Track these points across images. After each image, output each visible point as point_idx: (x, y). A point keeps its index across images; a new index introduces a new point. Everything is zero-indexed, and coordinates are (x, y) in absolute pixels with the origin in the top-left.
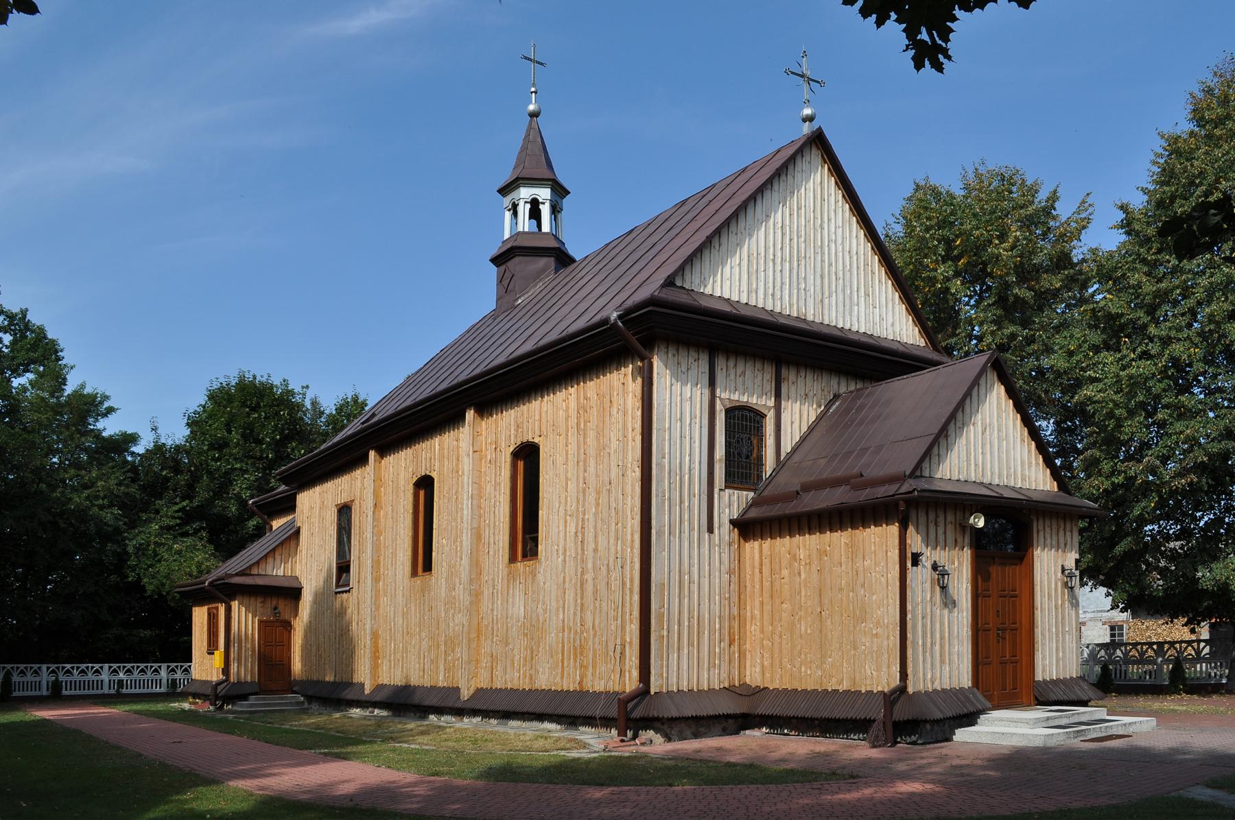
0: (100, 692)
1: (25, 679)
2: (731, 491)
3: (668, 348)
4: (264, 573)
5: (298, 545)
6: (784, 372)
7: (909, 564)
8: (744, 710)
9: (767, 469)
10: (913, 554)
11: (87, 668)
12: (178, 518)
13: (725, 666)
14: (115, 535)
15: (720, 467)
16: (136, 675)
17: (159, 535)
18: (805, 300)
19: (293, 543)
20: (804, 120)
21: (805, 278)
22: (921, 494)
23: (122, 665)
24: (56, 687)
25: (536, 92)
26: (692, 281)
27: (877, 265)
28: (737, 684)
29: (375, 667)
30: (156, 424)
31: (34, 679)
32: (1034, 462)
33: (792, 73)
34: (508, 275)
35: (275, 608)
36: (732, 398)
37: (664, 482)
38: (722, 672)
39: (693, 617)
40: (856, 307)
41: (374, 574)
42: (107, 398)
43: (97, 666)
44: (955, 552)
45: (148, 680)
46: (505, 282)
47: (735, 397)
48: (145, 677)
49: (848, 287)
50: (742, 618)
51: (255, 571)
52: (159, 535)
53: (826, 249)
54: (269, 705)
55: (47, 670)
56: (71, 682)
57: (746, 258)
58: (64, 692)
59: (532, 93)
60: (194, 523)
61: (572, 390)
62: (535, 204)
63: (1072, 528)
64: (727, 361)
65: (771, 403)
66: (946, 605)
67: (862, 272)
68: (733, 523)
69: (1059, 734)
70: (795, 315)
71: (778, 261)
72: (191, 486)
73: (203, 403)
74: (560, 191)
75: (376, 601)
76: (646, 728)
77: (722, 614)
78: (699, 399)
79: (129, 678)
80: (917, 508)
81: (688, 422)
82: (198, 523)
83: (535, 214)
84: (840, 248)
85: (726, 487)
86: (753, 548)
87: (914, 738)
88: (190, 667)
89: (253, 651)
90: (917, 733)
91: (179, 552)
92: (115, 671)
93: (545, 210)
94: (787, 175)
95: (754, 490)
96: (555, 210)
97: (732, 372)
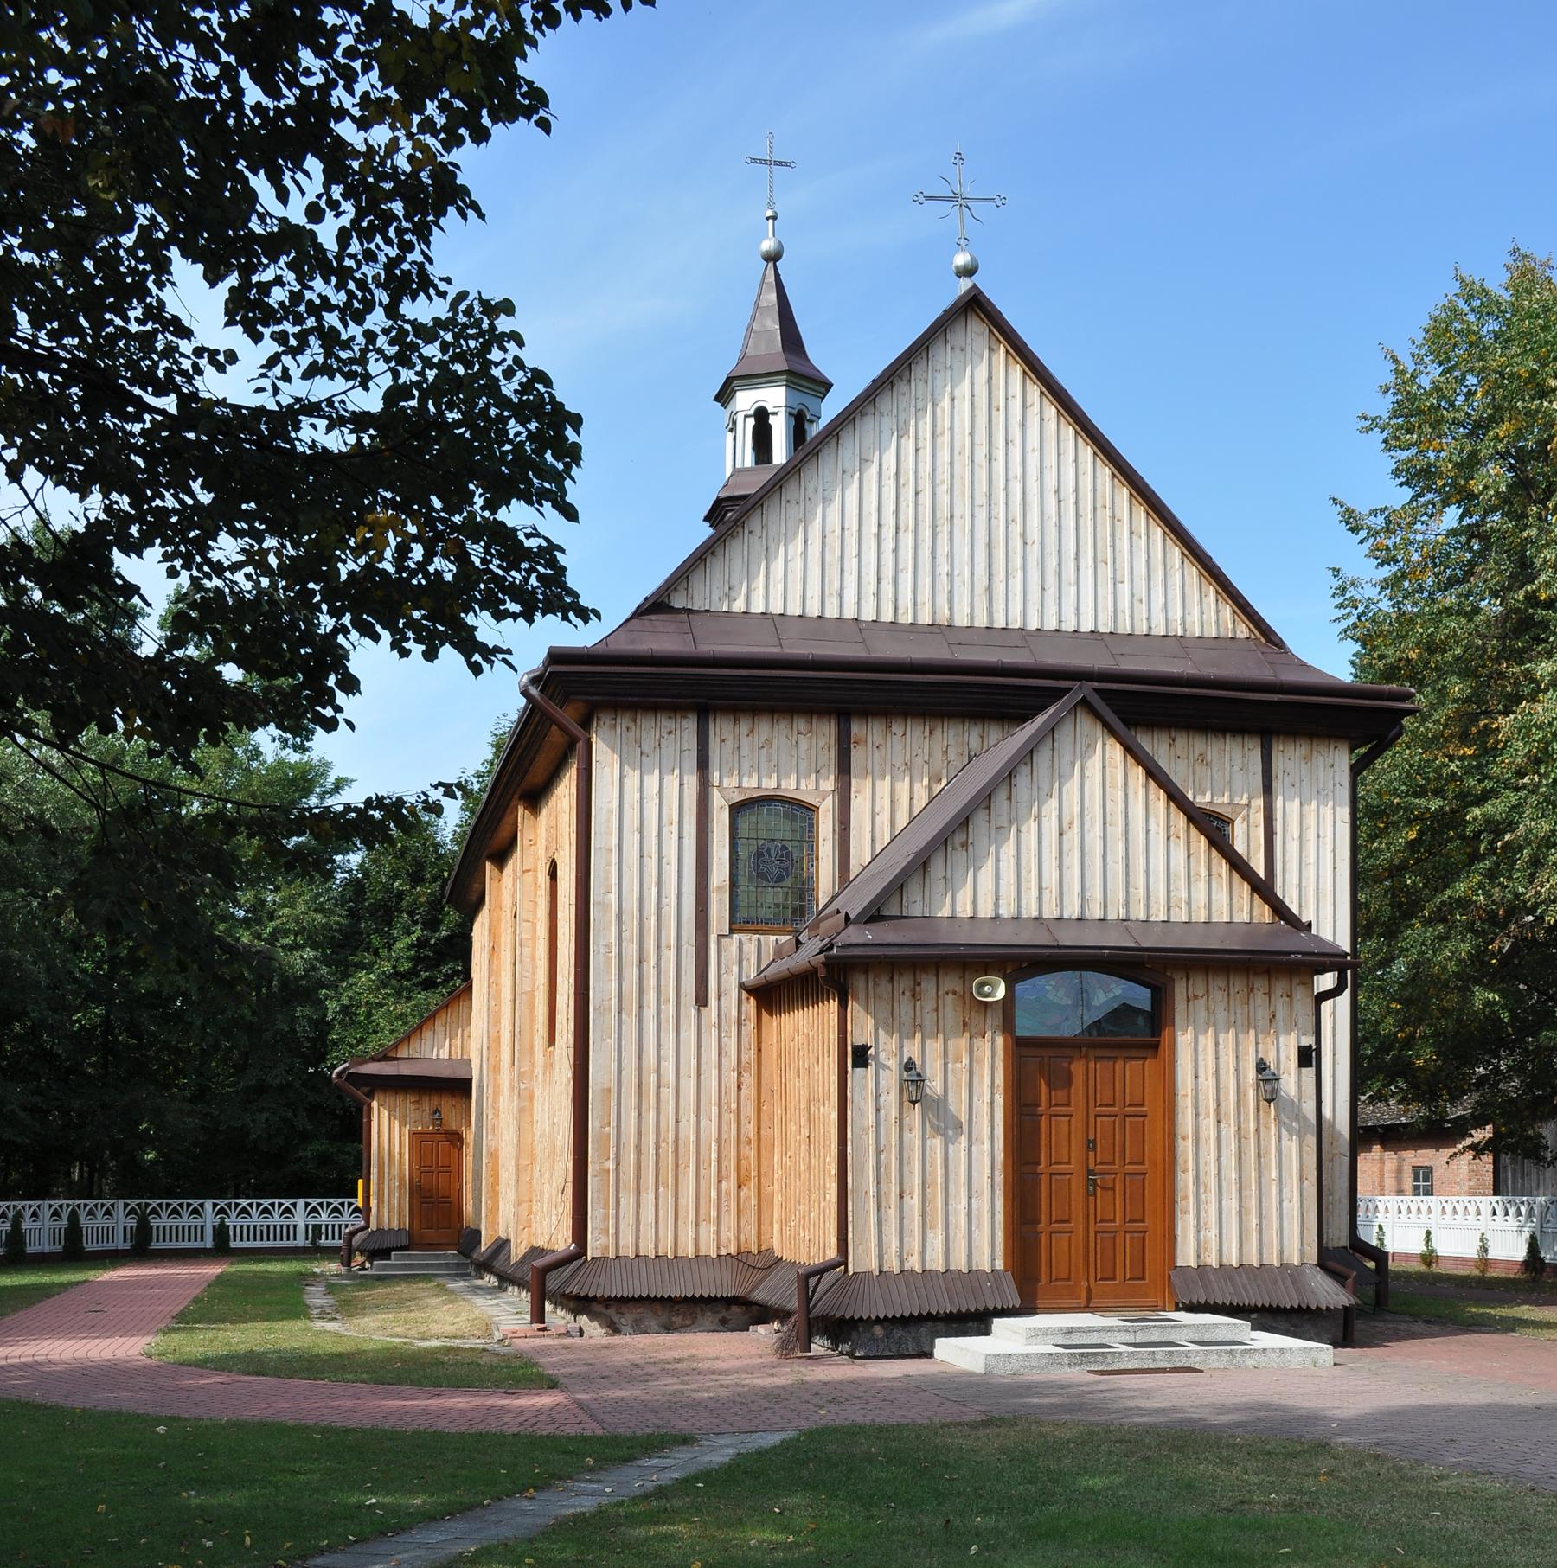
0: (291, 1243)
1: (179, 1222)
2: (744, 937)
4: (417, 1056)
6: (857, 728)
11: (229, 1205)
13: (730, 1220)
14: (304, 991)
16: (256, 1219)
18: (951, 592)
23: (325, 1200)
24: (221, 1233)
25: (774, 218)
26: (704, 595)
28: (754, 1250)
31: (193, 1223)
32: (1204, 873)
35: (437, 1111)
42: (328, 765)
43: (287, 1202)
47: (750, 782)
49: (1055, 554)
51: (403, 1052)
54: (411, 1266)
55: (125, 1208)
56: (248, 1227)
58: (232, 1244)
59: (768, 218)
62: (762, 416)
65: (829, 784)
69: (1198, 1352)
71: (889, 532)
73: (490, 757)
77: (724, 1136)
85: (732, 931)
86: (772, 1023)
89: (402, 1180)
93: (779, 427)
97: (745, 743)
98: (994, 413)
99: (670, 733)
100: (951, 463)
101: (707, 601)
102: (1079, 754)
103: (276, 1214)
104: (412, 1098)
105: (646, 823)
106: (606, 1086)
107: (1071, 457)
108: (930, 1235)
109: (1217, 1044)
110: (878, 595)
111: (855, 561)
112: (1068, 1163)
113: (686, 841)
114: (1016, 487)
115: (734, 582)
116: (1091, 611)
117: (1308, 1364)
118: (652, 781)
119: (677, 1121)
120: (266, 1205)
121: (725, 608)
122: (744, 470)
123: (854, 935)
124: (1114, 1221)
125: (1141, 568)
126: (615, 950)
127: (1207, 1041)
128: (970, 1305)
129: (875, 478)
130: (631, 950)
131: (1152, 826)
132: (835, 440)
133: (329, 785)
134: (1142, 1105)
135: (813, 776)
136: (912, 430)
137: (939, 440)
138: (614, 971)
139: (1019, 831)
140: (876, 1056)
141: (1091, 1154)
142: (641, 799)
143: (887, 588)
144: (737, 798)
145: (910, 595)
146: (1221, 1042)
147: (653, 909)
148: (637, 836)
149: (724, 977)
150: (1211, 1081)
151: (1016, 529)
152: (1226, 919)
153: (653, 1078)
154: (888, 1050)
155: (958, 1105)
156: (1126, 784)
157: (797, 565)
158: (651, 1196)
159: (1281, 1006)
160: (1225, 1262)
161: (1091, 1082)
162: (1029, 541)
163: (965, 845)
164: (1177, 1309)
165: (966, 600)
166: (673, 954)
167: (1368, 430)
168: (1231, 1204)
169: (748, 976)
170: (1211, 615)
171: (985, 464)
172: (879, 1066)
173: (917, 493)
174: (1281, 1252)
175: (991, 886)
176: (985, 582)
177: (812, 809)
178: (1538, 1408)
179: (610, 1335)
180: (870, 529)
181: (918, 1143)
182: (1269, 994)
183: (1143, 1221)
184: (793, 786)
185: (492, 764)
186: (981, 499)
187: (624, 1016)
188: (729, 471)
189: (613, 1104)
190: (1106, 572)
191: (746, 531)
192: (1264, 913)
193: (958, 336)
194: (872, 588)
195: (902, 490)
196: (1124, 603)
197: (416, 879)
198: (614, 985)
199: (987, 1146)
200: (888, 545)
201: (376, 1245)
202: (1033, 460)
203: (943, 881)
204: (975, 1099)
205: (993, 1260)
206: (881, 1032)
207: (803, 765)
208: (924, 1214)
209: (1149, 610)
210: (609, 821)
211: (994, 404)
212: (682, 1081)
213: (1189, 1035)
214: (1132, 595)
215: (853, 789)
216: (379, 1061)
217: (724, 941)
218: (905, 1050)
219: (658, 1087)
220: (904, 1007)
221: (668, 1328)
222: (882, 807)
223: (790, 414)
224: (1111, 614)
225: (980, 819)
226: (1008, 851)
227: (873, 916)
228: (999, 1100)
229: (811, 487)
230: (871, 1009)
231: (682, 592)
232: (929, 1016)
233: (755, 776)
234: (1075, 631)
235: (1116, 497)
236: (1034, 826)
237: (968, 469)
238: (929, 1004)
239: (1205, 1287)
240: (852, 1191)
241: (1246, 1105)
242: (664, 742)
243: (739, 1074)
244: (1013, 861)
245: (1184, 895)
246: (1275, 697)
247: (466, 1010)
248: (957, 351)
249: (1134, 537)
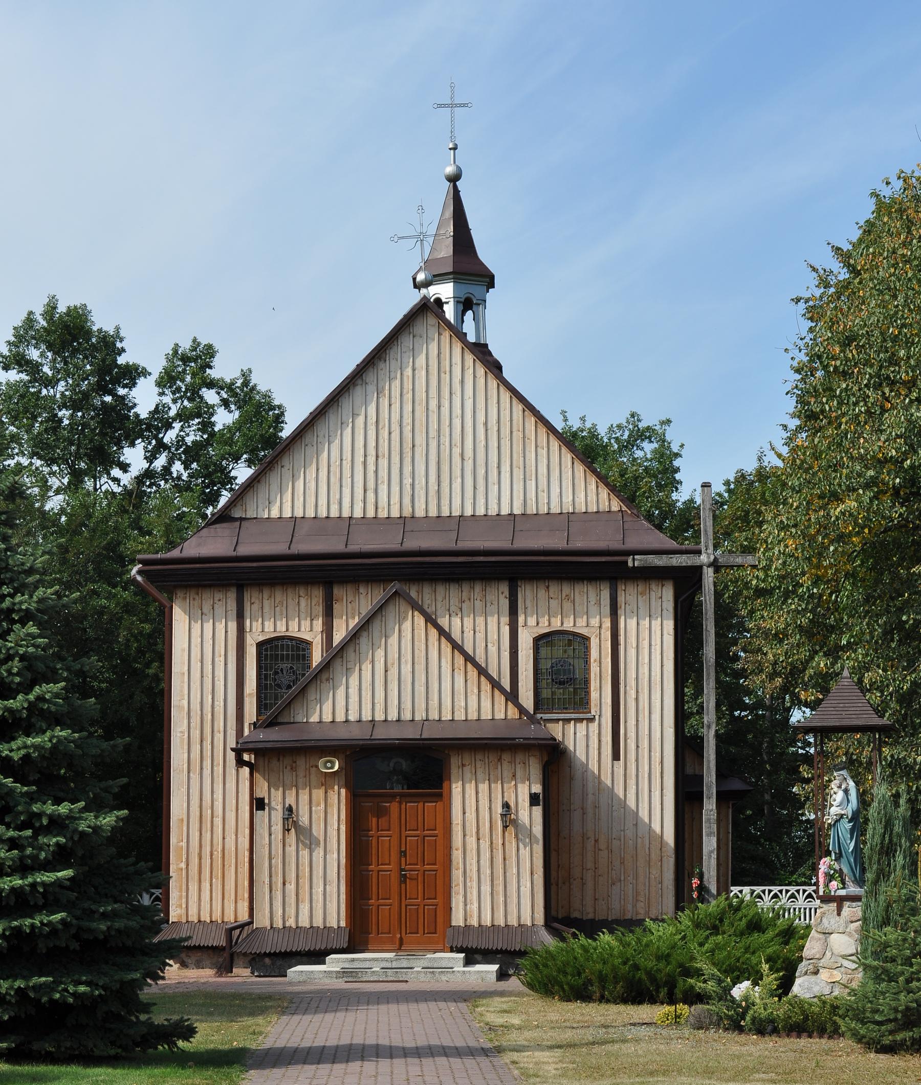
18: (413, 495)
59: (450, 149)
65: (319, 624)
71: (371, 460)
98: (442, 375)
99: (219, 600)
108: (301, 906)
109: (477, 793)
112: (389, 864)
114: (457, 423)
118: (208, 626)
119: (224, 838)
120: (157, 894)
125: (543, 470)
126: (186, 735)
127: (470, 789)
130: (196, 734)
136: (387, 392)
138: (186, 747)
139: (360, 670)
141: (403, 859)
142: (202, 641)
143: (371, 496)
144: (261, 638)
145: (386, 499)
146: (480, 791)
147: (210, 709)
151: (457, 451)
153: (209, 812)
155: (318, 831)
160: (483, 923)
165: (423, 500)
168: (486, 888)
170: (592, 497)
174: (519, 918)
178: (475, 992)
180: (359, 459)
181: (294, 854)
183: (435, 899)
186: (433, 433)
189: (185, 828)
190: (518, 474)
193: (420, 327)
196: (532, 494)
198: (186, 755)
199: (335, 855)
200: (371, 468)
205: (339, 921)
208: (297, 895)
211: (442, 370)
219: (212, 817)
223: (458, 302)
226: (354, 681)
228: (343, 828)
231: (239, 507)
234: (497, 515)
235: (526, 424)
242: (216, 606)
244: (357, 688)
246: (603, 559)
249: (539, 449)
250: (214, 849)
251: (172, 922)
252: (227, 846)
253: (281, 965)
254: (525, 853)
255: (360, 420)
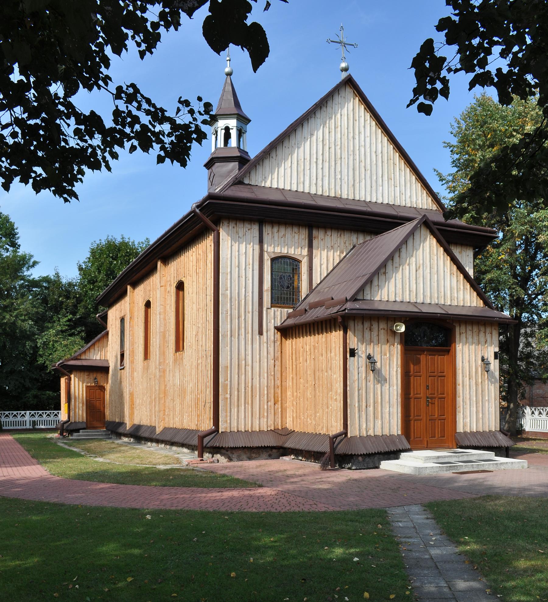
1: (17, 419)
2: (276, 309)
3: (229, 223)
4: (88, 358)
5: (108, 341)
6: (315, 233)
7: (348, 356)
8: (279, 444)
9: (302, 294)
10: (350, 349)
11: (51, 413)
12: (67, 325)
13: (271, 417)
14: (30, 336)
15: (267, 295)
16: (11, 419)
17: (56, 335)
18: (341, 185)
19: (105, 340)
20: (342, 71)
21: (341, 172)
22: (351, 312)
25: (230, 60)
27: (398, 159)
28: (280, 428)
29: (132, 414)
30: (58, 271)
32: (462, 288)
33: (332, 41)
34: (212, 175)
35: (95, 379)
36: (276, 251)
37: (228, 305)
38: (269, 420)
39: (248, 387)
40: (381, 188)
41: (131, 359)
42: (32, 256)
43: (23, 412)
44: (386, 347)
45: (52, 421)
46: (211, 180)
47: (278, 250)
48: (50, 419)
49: (375, 175)
50: (283, 388)
51: (83, 357)
52: (56, 335)
53: (357, 152)
57: (296, 163)
59: (227, 60)
60: (78, 327)
61: (194, 249)
62: (227, 129)
63: (492, 332)
64: (272, 228)
65: (305, 252)
66: (379, 382)
67: (386, 165)
68: (277, 328)
70: (333, 195)
71: (320, 162)
72: (75, 306)
73: (89, 256)
74: (243, 120)
75: (131, 374)
76: (217, 453)
77: (269, 385)
78: (251, 253)
79: (41, 419)
80: (354, 320)
81: (244, 268)
82: (80, 328)
83: (227, 136)
84: (368, 150)
85: (271, 307)
86: (289, 343)
87: (350, 465)
88: (58, 413)
90: (351, 462)
91: (66, 346)
92: (33, 415)
93: (234, 133)
94: (327, 107)
95: (293, 308)
96: (240, 133)
97: (276, 235)
98: (355, 122)
99: (249, 230)
100: (341, 138)
101: (257, 182)
102: (422, 241)
103: (19, 417)
104: (86, 374)
105: (240, 264)
106: (226, 365)
107: (380, 141)
110: (316, 184)
111: (308, 171)
113: (255, 271)
115: (266, 175)
116: (387, 196)
117: (520, 468)
118: (243, 246)
121: (263, 185)
122: (221, 148)
123: (349, 305)
124: (435, 416)
125: (403, 182)
126: (229, 313)
128: (393, 448)
129: (315, 141)
131: (446, 270)
132: (301, 126)
133: (31, 263)
134: (443, 373)
135: (300, 248)
136: (327, 125)
137: (336, 129)
140: (358, 353)
142: (239, 254)
144: (273, 256)
148: (237, 269)
149: (269, 324)
150: (467, 364)
151: (363, 164)
152: (469, 305)
153: (243, 362)
154: (362, 350)
155: (385, 372)
156: (437, 254)
157: (289, 171)
158: (243, 407)
159: (488, 336)
160: (472, 431)
161: (427, 364)
162: (367, 170)
163: (385, 273)
164: (457, 448)
166: (250, 315)
167: (446, 147)
169: (277, 324)
171: (352, 140)
172: (359, 356)
173: (329, 148)
175: (393, 289)
176: (352, 183)
177: (300, 262)
179: (229, 462)
181: (372, 386)
182: (485, 332)
184: (293, 253)
185: (89, 258)
187: (232, 338)
188: (213, 149)
189: (229, 372)
191: (271, 157)
192: (481, 303)
193: (342, 93)
194: (314, 182)
195: (324, 147)
196: (398, 194)
197: (68, 297)
198: (229, 326)
199: (395, 388)
200: (320, 166)
201: (72, 427)
202: (368, 140)
203: (377, 287)
204: (391, 370)
206: (359, 343)
207: (297, 245)
209: (405, 197)
210: (227, 262)
212: (254, 364)
213: (461, 347)
214: (400, 192)
215: (314, 255)
216: (75, 360)
217: (268, 310)
218: (367, 350)
219: (245, 366)
220: (367, 334)
221: (250, 459)
222: (324, 262)
224: (393, 198)
225: (390, 264)
227: (354, 299)
229: (293, 143)
230: (356, 334)
232: (375, 338)
233: (286, 247)
236: (407, 267)
237: (346, 141)
238: (375, 333)
239: (468, 440)
240: (350, 405)
241: (478, 373)
242: (247, 233)
243: (275, 361)
244: (401, 280)
245: (456, 295)
246: (456, 230)
247: (106, 342)
248: (343, 98)
250: (247, 386)
251: (222, 432)
252: (254, 384)
253: (368, 461)
254: (492, 388)
255: (314, 138)
